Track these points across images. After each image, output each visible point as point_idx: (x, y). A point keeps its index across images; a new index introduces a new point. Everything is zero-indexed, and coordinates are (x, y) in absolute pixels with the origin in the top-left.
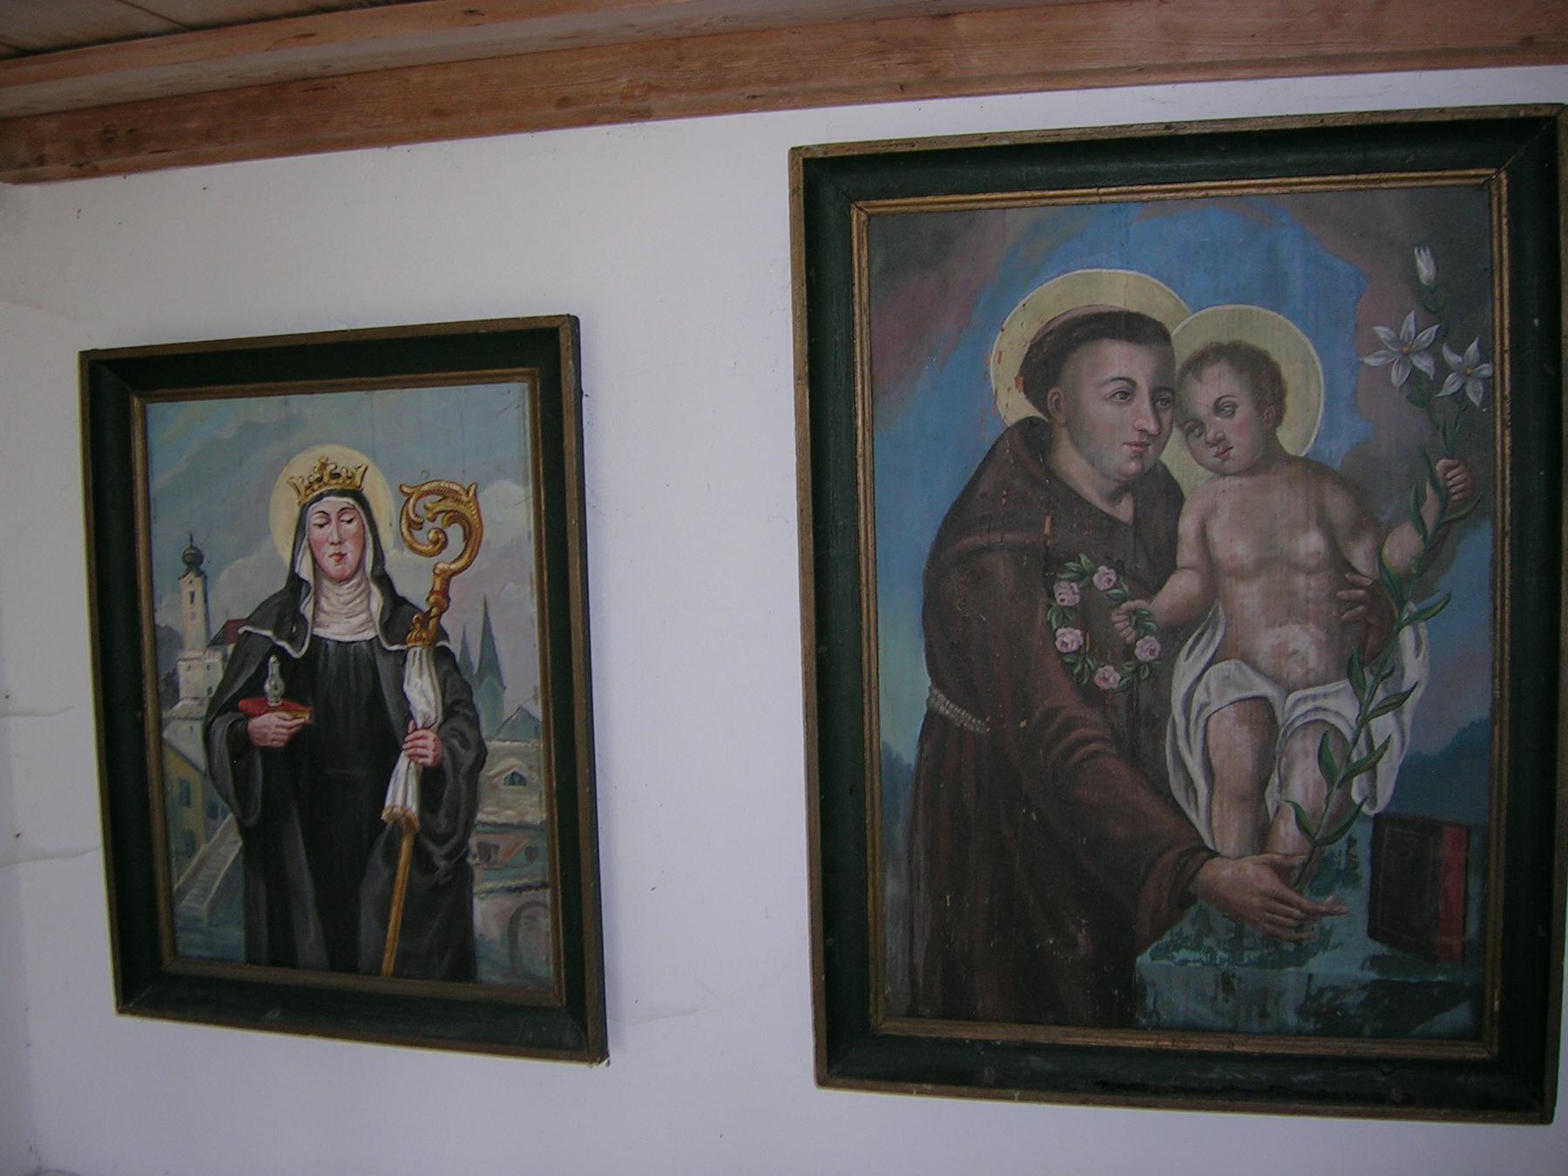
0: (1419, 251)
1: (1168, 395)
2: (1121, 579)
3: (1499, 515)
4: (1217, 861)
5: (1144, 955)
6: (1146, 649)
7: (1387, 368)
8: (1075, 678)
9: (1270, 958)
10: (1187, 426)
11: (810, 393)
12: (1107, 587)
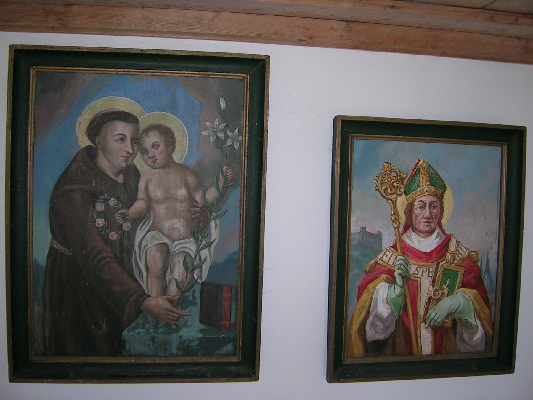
2: (118, 202)
4: (150, 299)
5: (125, 331)
6: (126, 226)
7: (209, 136)
8: (102, 236)
10: (143, 151)
11: (11, 132)
12: (114, 205)
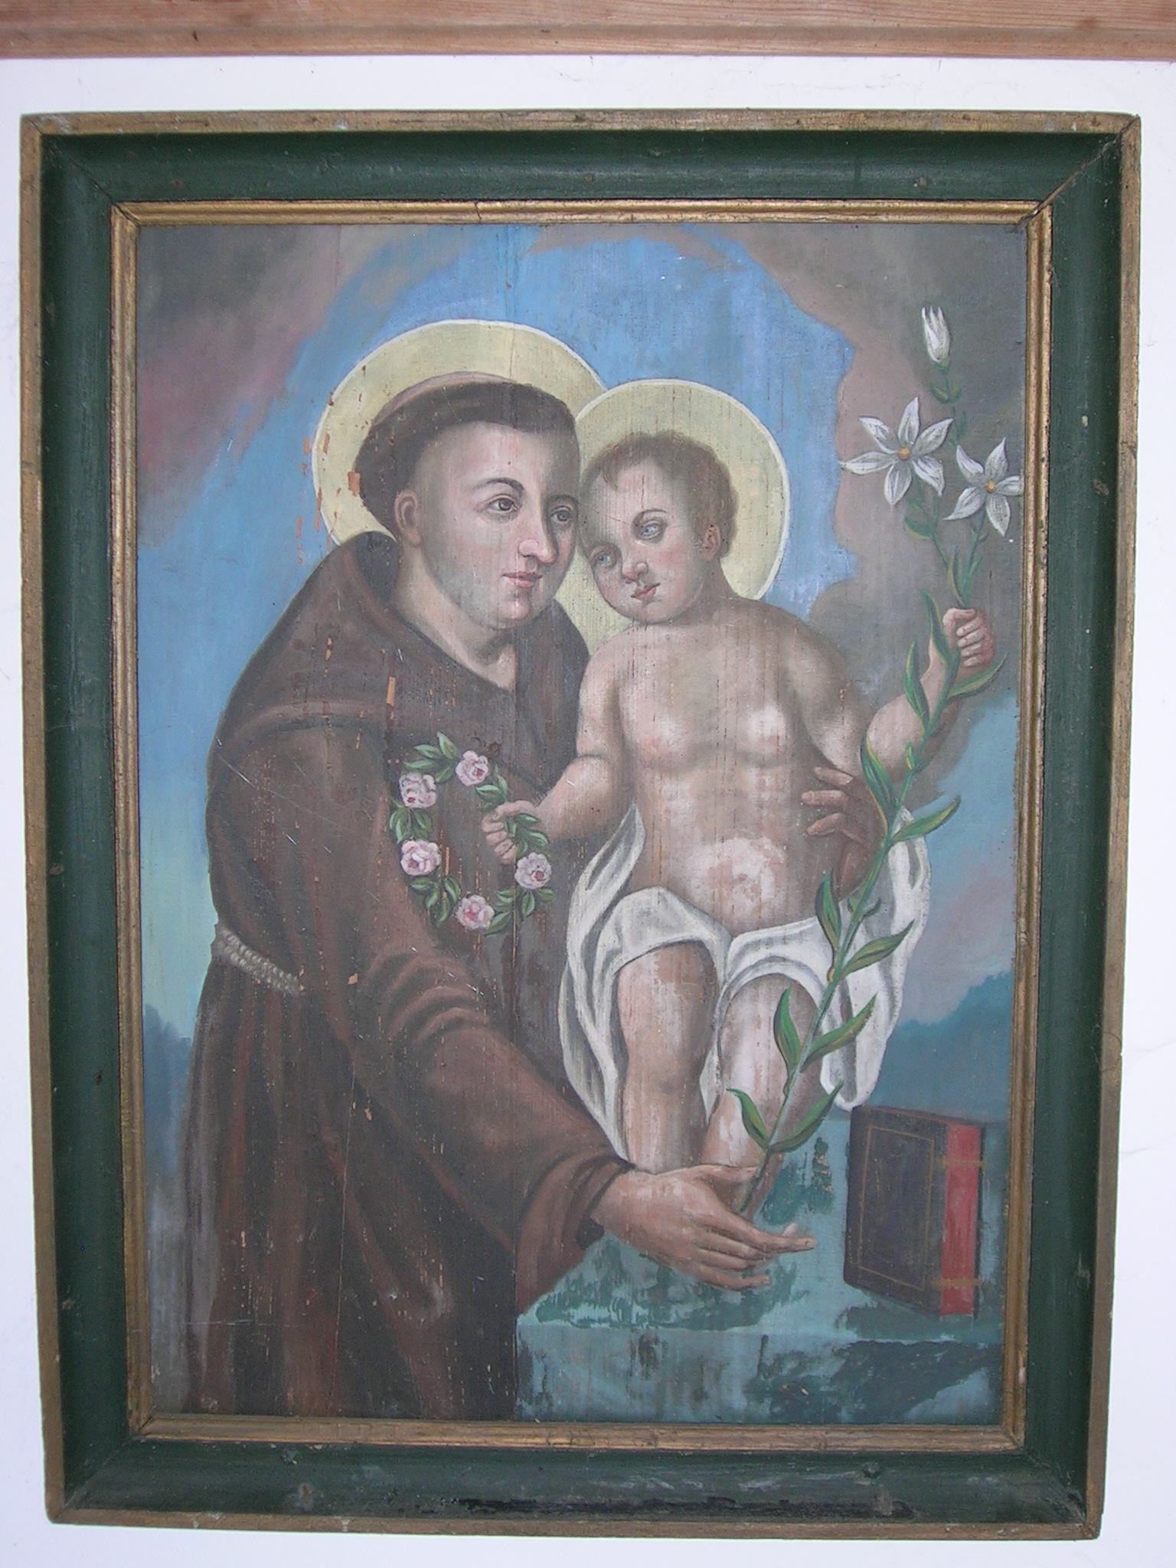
0: (927, 314)
1: (569, 506)
2: (497, 769)
3: (1029, 688)
4: (632, 1176)
6: (532, 870)
9: (709, 1314)
10: (594, 552)
12: (477, 782)
